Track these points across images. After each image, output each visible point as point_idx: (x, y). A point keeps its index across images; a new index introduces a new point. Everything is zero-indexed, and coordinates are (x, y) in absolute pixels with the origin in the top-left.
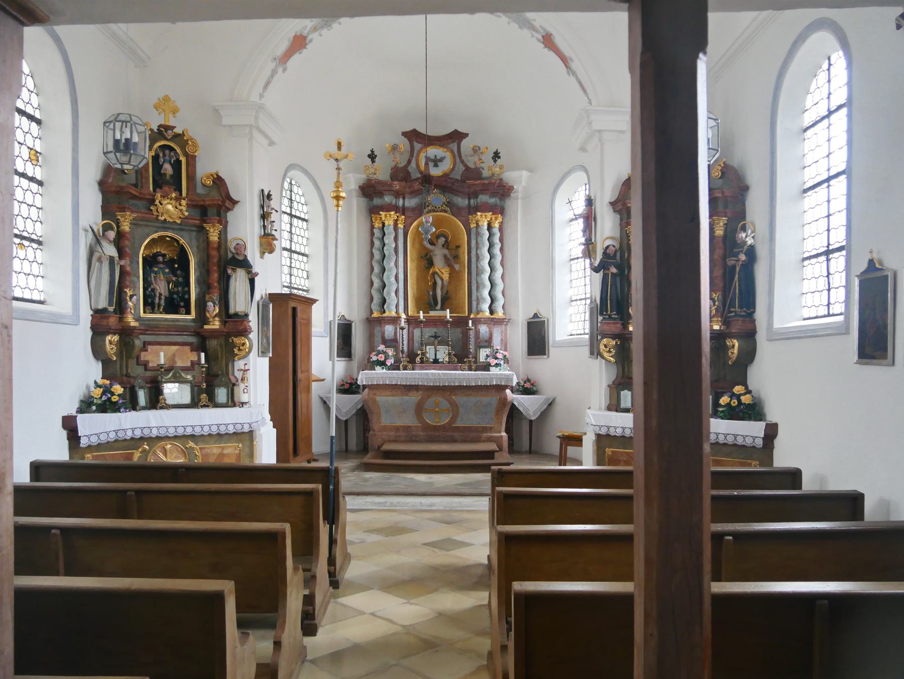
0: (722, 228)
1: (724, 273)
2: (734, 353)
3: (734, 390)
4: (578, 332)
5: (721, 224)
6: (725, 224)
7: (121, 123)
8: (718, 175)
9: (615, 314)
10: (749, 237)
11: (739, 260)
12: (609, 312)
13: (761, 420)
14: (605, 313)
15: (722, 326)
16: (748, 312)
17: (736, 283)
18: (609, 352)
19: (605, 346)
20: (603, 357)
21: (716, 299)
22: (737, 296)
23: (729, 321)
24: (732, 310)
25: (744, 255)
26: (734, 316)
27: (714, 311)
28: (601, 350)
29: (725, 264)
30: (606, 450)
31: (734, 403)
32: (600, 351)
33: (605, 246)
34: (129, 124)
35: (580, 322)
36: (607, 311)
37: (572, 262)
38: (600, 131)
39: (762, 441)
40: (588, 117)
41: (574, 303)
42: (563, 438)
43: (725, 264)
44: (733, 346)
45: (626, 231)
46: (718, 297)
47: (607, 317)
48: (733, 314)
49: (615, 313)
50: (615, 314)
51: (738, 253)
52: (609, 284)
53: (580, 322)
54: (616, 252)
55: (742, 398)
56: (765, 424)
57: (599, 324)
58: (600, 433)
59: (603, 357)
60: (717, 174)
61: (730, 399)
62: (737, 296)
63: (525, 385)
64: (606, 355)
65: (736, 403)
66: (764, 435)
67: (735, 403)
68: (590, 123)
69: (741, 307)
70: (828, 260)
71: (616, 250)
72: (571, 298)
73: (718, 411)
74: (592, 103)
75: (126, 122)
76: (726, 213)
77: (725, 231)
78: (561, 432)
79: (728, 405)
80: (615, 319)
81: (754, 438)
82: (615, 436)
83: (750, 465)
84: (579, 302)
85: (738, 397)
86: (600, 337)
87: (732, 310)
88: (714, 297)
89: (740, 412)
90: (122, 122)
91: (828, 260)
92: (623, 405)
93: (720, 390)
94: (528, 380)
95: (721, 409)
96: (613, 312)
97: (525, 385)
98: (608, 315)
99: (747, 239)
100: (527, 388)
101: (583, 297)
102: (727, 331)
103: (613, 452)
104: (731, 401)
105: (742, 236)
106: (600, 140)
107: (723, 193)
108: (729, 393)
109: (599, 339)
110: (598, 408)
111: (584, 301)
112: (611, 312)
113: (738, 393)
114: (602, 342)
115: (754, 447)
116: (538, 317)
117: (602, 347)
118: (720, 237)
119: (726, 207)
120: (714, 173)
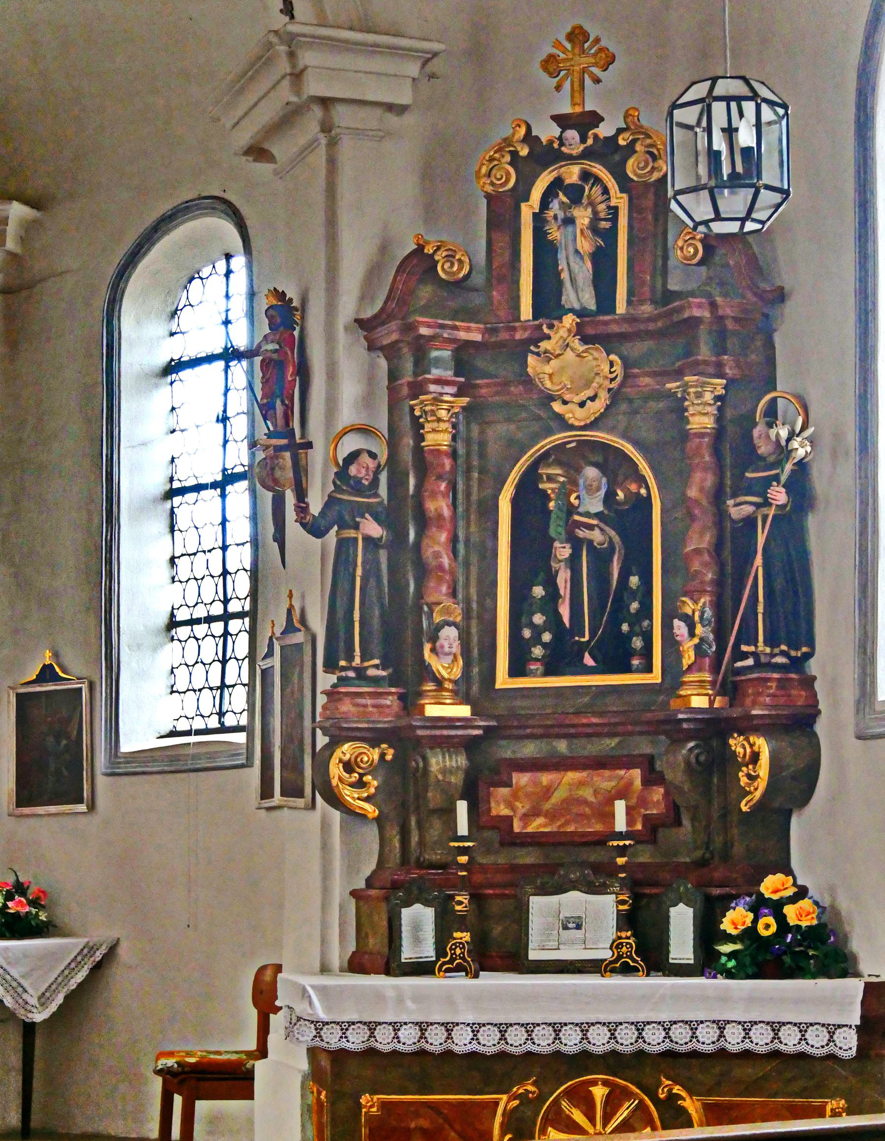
0: (709, 409)
1: (718, 546)
2: (758, 776)
3: (762, 889)
4: (199, 724)
5: (708, 397)
6: (718, 398)
7: (724, 104)
8: (696, 251)
9: (376, 666)
10: (799, 439)
11: (771, 505)
12: (357, 661)
13: (844, 974)
14: (343, 663)
15: (718, 698)
16: (793, 653)
17: (758, 567)
18: (360, 784)
19: (348, 767)
20: (334, 800)
21: (697, 618)
22: (760, 609)
23: (736, 686)
24: (744, 648)
25: (783, 490)
26: (749, 668)
27: (692, 653)
28: (335, 782)
29: (721, 515)
30: (363, 1101)
31: (767, 926)
32: (330, 782)
33: (341, 456)
34: (749, 107)
35: (206, 692)
36: (350, 658)
37: (177, 500)
38: (325, 102)
39: (855, 1037)
40: (292, 55)
41: (183, 632)
42: (183, 1073)
43: (721, 515)
44: (755, 758)
45: (412, 409)
46: (702, 613)
47: (351, 674)
48: (750, 662)
49: (376, 661)
50: (376, 666)
51: (767, 483)
52: (359, 572)
53: (206, 692)
54: (378, 470)
55: (790, 911)
56: (862, 986)
57: (321, 700)
58: (344, 1044)
59: (334, 800)
60: (692, 250)
61: (751, 916)
62: (760, 609)
63: (10, 904)
64: (349, 795)
65: (774, 928)
66: (863, 1017)
67: (767, 926)
68: (297, 76)
69: (771, 641)
70: (223, 496)
71: (379, 466)
72: (172, 615)
73: (720, 954)
74: (295, 13)
75: (739, 99)
76: (719, 365)
77: (719, 419)
78: (171, 1054)
79: (750, 934)
80: (376, 681)
81: (832, 1029)
82: (395, 1052)
83: (820, 1113)
84: (200, 630)
85: (777, 908)
86: (326, 740)
87: (744, 648)
88: (690, 612)
89: (785, 953)
90: (728, 99)
91: (223, 496)
92: (407, 954)
93: (716, 891)
94: (20, 888)
95: (726, 948)
96: (372, 658)
97: (10, 904)
98: (356, 669)
99: (795, 444)
100: (17, 915)
101: (217, 609)
102: (736, 712)
103: (384, 1105)
104: (755, 921)
105: (778, 435)
106: (326, 127)
107: (713, 305)
108: (748, 899)
109: (319, 746)
110: (317, 966)
111: (221, 624)
112: (363, 660)
113: (775, 897)
114: (338, 754)
115: (832, 1057)
116: (56, 678)
117: (335, 770)
118: (702, 435)
119: (720, 348)
120: (682, 249)
